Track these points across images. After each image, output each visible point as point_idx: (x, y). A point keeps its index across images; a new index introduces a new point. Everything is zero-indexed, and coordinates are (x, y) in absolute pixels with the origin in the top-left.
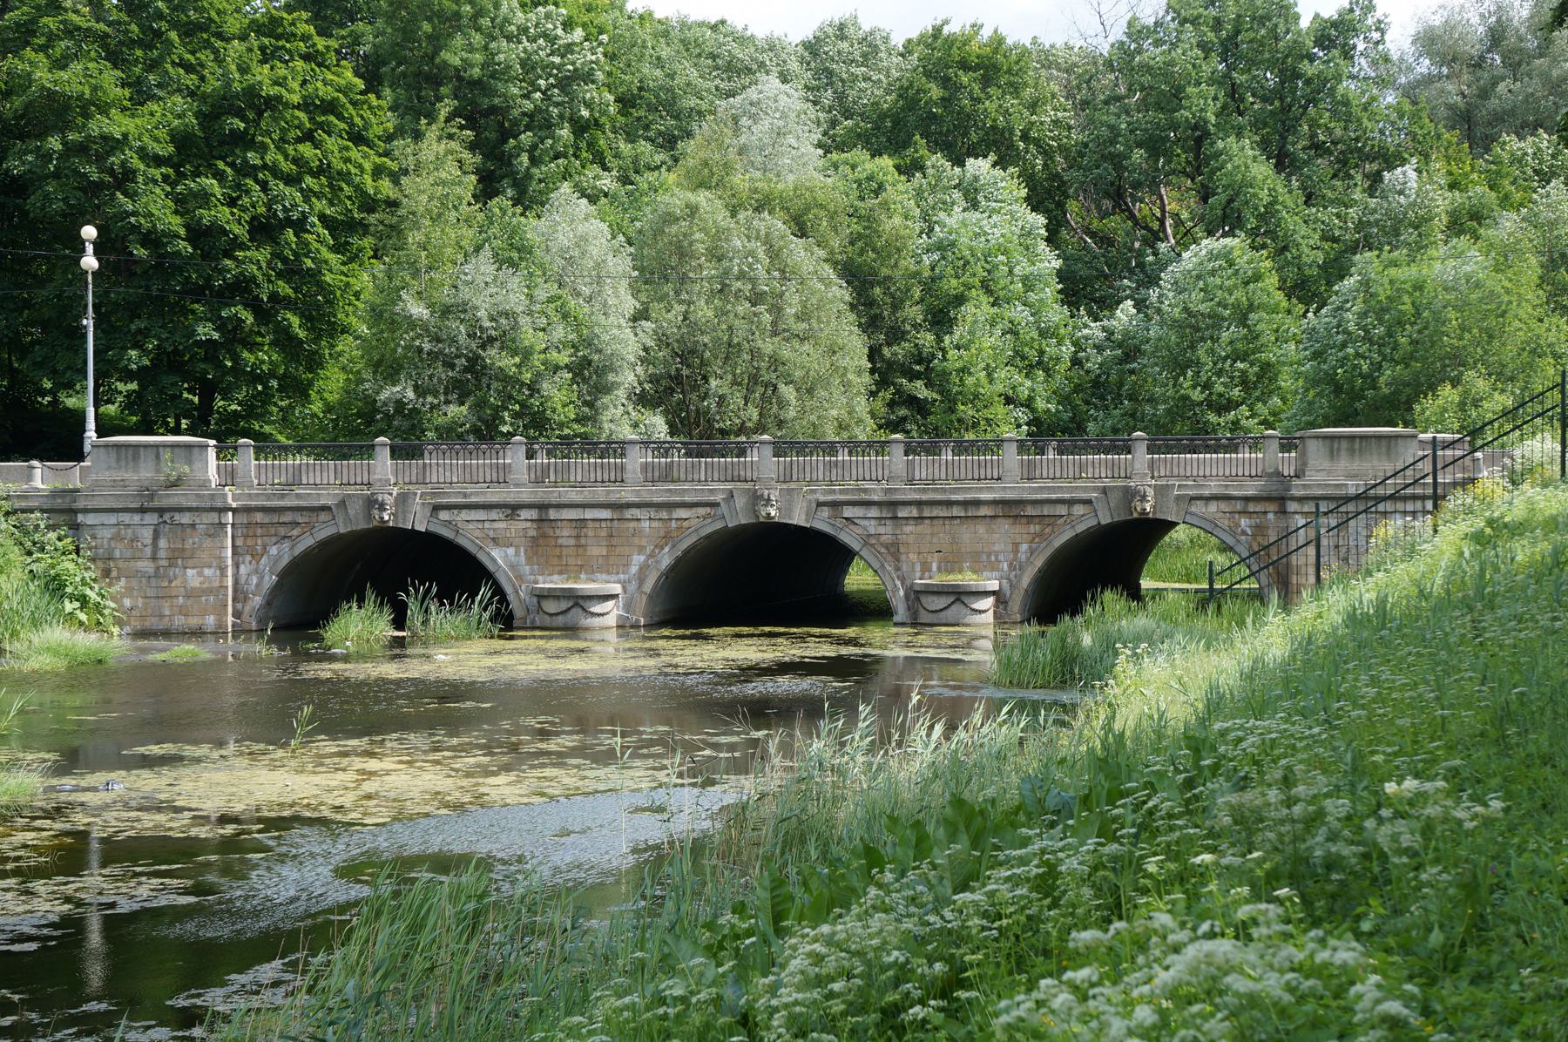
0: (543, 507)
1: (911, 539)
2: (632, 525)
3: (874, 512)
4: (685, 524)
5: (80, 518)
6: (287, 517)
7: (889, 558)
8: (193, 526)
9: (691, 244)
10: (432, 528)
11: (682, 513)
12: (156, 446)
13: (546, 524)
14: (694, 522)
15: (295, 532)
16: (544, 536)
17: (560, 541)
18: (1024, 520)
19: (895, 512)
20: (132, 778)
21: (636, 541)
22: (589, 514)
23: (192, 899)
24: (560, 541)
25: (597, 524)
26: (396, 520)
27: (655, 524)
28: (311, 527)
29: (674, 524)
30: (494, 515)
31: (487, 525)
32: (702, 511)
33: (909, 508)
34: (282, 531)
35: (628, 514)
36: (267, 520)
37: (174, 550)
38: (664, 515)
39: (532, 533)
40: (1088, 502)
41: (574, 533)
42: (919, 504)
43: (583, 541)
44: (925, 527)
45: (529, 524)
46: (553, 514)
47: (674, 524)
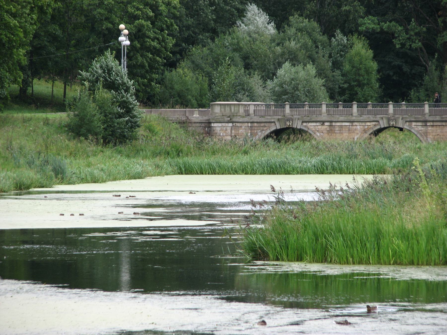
0: (331, 122)
1: (430, 131)
2: (355, 127)
3: (420, 124)
4: (370, 127)
5: (212, 125)
6: (262, 125)
7: (425, 136)
8: (241, 127)
9: (283, 79)
10: (301, 128)
11: (368, 124)
12: (231, 104)
13: (332, 127)
14: (372, 126)
15: (265, 129)
16: (331, 130)
17: (336, 132)
18: (435, 126)
19: (352, 124)
20: (331, 273)
21: (356, 132)
22: (344, 124)
23: (327, 306)
24: (336, 132)
25: (346, 127)
26: (292, 126)
27: (361, 127)
28: (269, 127)
29: (366, 127)
30: (318, 124)
31: (316, 127)
32: (374, 123)
33: (430, 123)
34: (261, 128)
35: (355, 124)
36: (258, 125)
37: (236, 133)
38: (364, 124)
39: (328, 129)
40: (274, 122)
41: (339, 129)
42: (433, 121)
43: (342, 132)
44: (434, 128)
45: (327, 127)
46: (334, 124)
47: (366, 127)
